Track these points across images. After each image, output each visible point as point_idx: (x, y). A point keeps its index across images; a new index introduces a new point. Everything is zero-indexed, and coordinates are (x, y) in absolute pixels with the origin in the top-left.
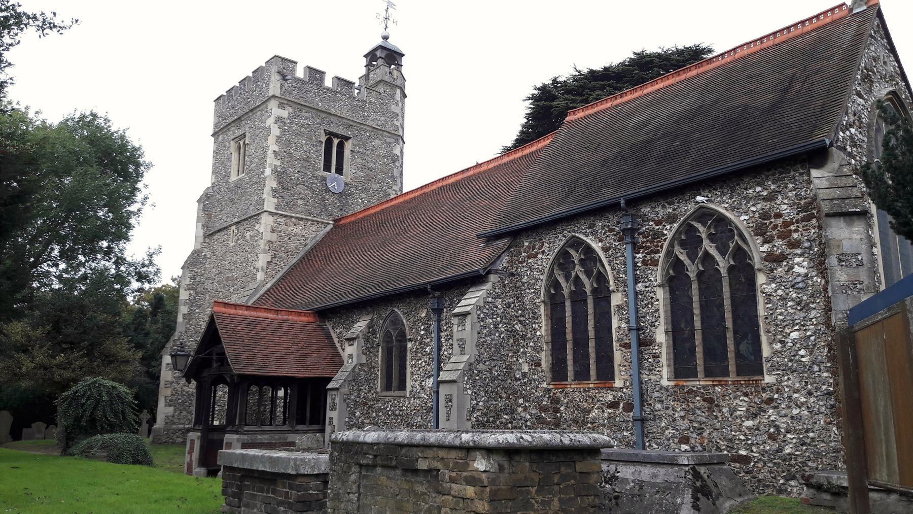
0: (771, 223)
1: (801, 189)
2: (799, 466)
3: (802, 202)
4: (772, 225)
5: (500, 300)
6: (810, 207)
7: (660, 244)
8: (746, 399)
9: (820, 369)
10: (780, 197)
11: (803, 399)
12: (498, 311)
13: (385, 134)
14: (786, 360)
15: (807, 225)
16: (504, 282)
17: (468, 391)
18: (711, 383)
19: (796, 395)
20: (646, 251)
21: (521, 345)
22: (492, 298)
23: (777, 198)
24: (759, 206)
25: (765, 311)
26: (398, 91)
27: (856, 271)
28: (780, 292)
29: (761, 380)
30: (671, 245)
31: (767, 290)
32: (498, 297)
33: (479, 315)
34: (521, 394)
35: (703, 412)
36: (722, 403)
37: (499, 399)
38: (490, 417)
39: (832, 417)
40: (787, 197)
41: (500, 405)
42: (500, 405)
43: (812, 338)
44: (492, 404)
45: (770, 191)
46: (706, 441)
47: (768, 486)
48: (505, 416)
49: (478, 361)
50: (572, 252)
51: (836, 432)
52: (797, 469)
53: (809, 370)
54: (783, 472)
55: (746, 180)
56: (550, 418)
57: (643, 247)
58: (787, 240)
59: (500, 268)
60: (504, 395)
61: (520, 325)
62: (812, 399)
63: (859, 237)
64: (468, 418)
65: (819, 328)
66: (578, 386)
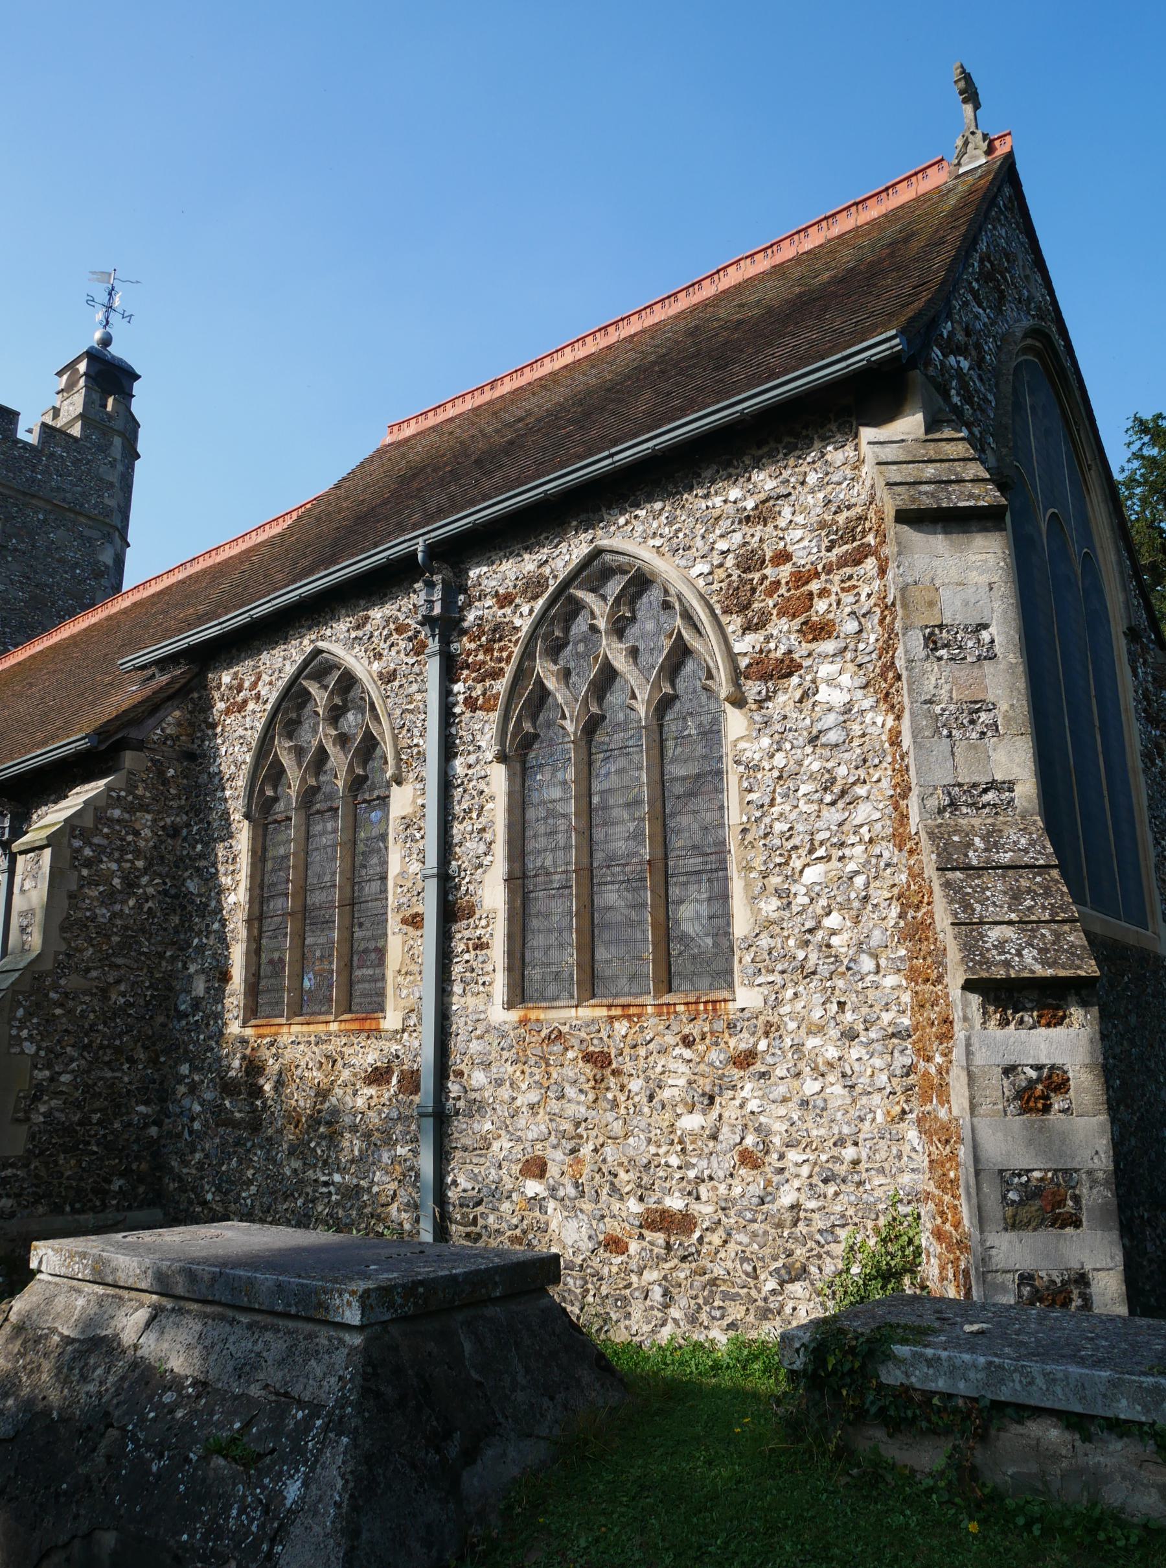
0: (765, 577)
1: (840, 483)
2: (818, 1242)
3: (841, 519)
4: (767, 583)
5: (149, 817)
6: (860, 528)
7: (505, 654)
8: (688, 1054)
9: (878, 966)
10: (787, 511)
11: (832, 1053)
12: (142, 844)
13: (83, 520)
14: (791, 942)
15: (850, 577)
16: (161, 773)
17: (26, 1044)
18: (604, 1012)
19: (812, 1042)
20: (473, 675)
21: (196, 928)
22: (125, 810)
23: (780, 513)
24: (737, 538)
25: (741, 812)
26: (117, 441)
27: (976, 672)
28: (779, 760)
29: (725, 1001)
30: (528, 654)
31: (748, 754)
32: (145, 808)
33: (79, 850)
34: (186, 1051)
35: (581, 1091)
36: (628, 1067)
37: (126, 1066)
38: (95, 1111)
39: (907, 1101)
40: (805, 510)
41: (126, 1079)
42: (126, 1079)
43: (860, 881)
44: (100, 1079)
45: (762, 496)
46: (586, 1171)
47: (734, 1298)
48: (142, 1109)
49: (61, 968)
50: (313, 688)
51: (915, 1142)
52: (811, 1250)
53: (849, 969)
54: (775, 1258)
55: (708, 473)
56: (239, 1111)
57: (468, 667)
58: (802, 619)
59: (156, 737)
60: (141, 1055)
61: (196, 880)
62: (856, 1052)
63: (984, 579)
64: (21, 1115)
65: (877, 851)
66: (305, 1028)
